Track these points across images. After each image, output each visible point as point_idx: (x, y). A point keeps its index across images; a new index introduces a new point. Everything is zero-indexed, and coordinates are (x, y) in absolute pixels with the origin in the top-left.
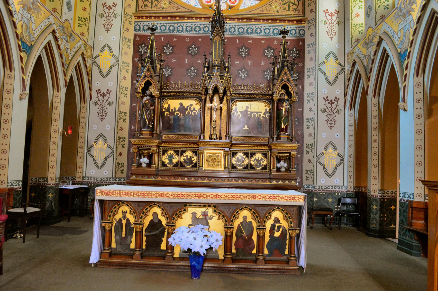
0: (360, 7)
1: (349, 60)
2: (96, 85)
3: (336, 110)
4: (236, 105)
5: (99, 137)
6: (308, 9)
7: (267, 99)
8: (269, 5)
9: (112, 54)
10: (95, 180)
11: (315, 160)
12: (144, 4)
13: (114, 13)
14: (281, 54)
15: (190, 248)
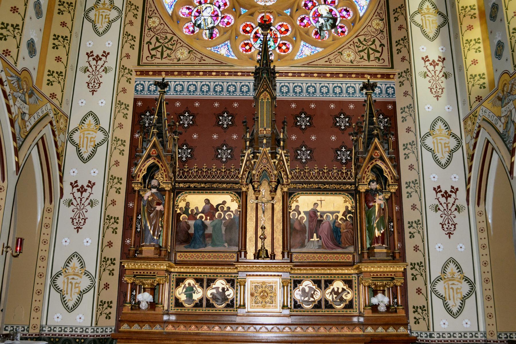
0: (478, 50)
1: (469, 129)
2: (70, 175)
3: (454, 207)
4: (297, 201)
5: (72, 258)
6: (397, 58)
7: (347, 191)
8: (339, 52)
9: (98, 126)
10: (61, 331)
11: (429, 289)
12: (151, 54)
13: (104, 66)
14: (367, 118)
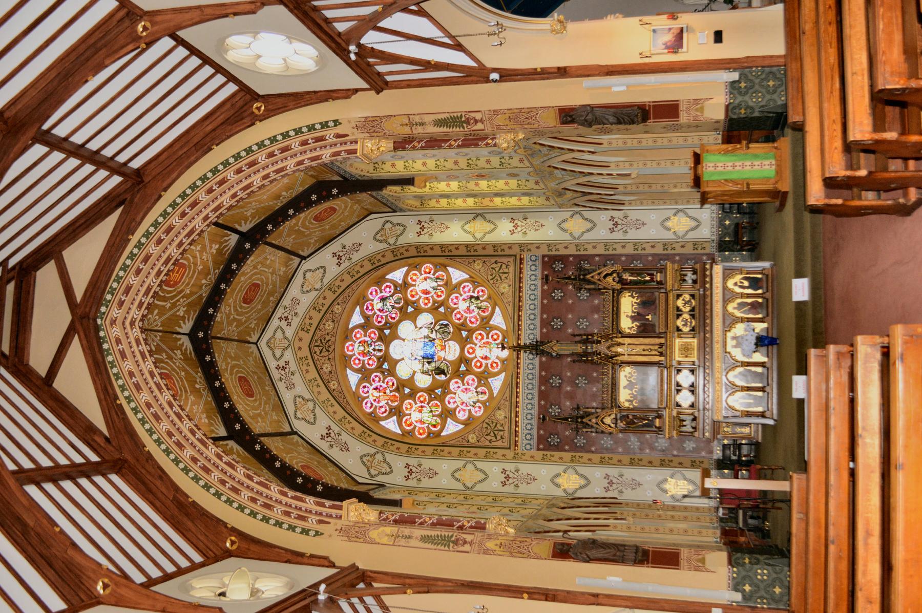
6: (507, 252)
7: (618, 296)
9: (563, 474)
15: (754, 341)
